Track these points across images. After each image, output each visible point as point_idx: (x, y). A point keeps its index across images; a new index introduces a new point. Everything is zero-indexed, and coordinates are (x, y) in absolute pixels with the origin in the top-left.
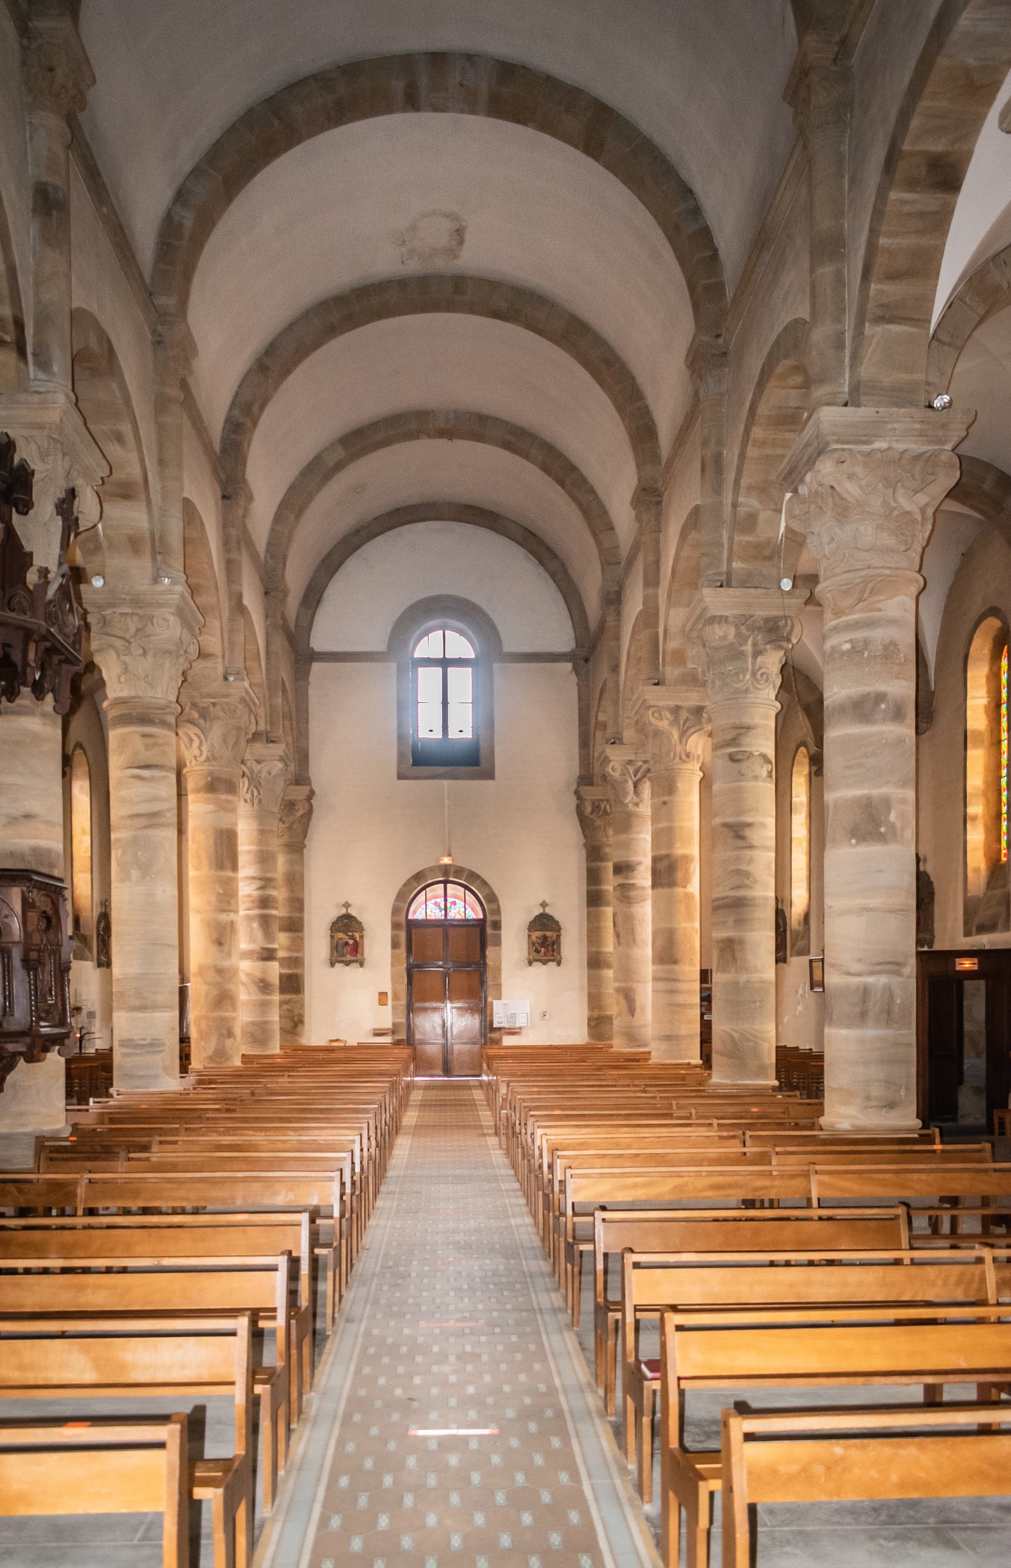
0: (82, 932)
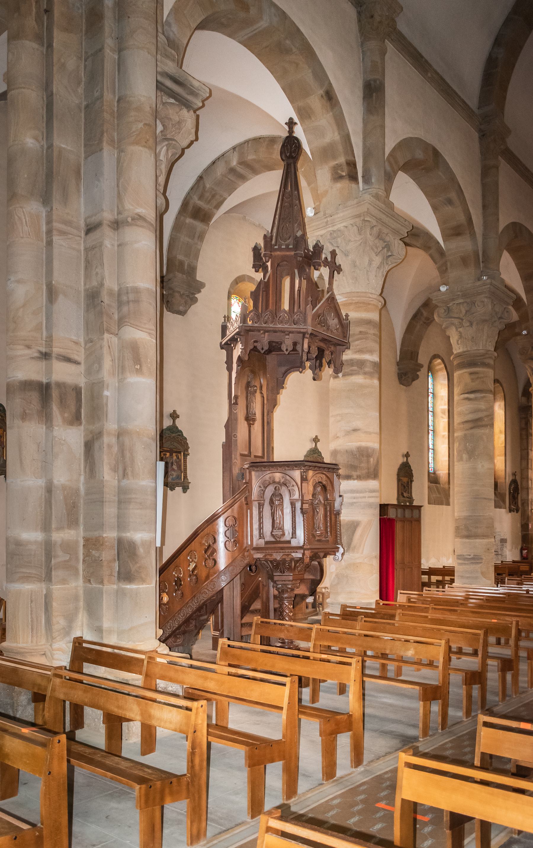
0: (499, 491)
